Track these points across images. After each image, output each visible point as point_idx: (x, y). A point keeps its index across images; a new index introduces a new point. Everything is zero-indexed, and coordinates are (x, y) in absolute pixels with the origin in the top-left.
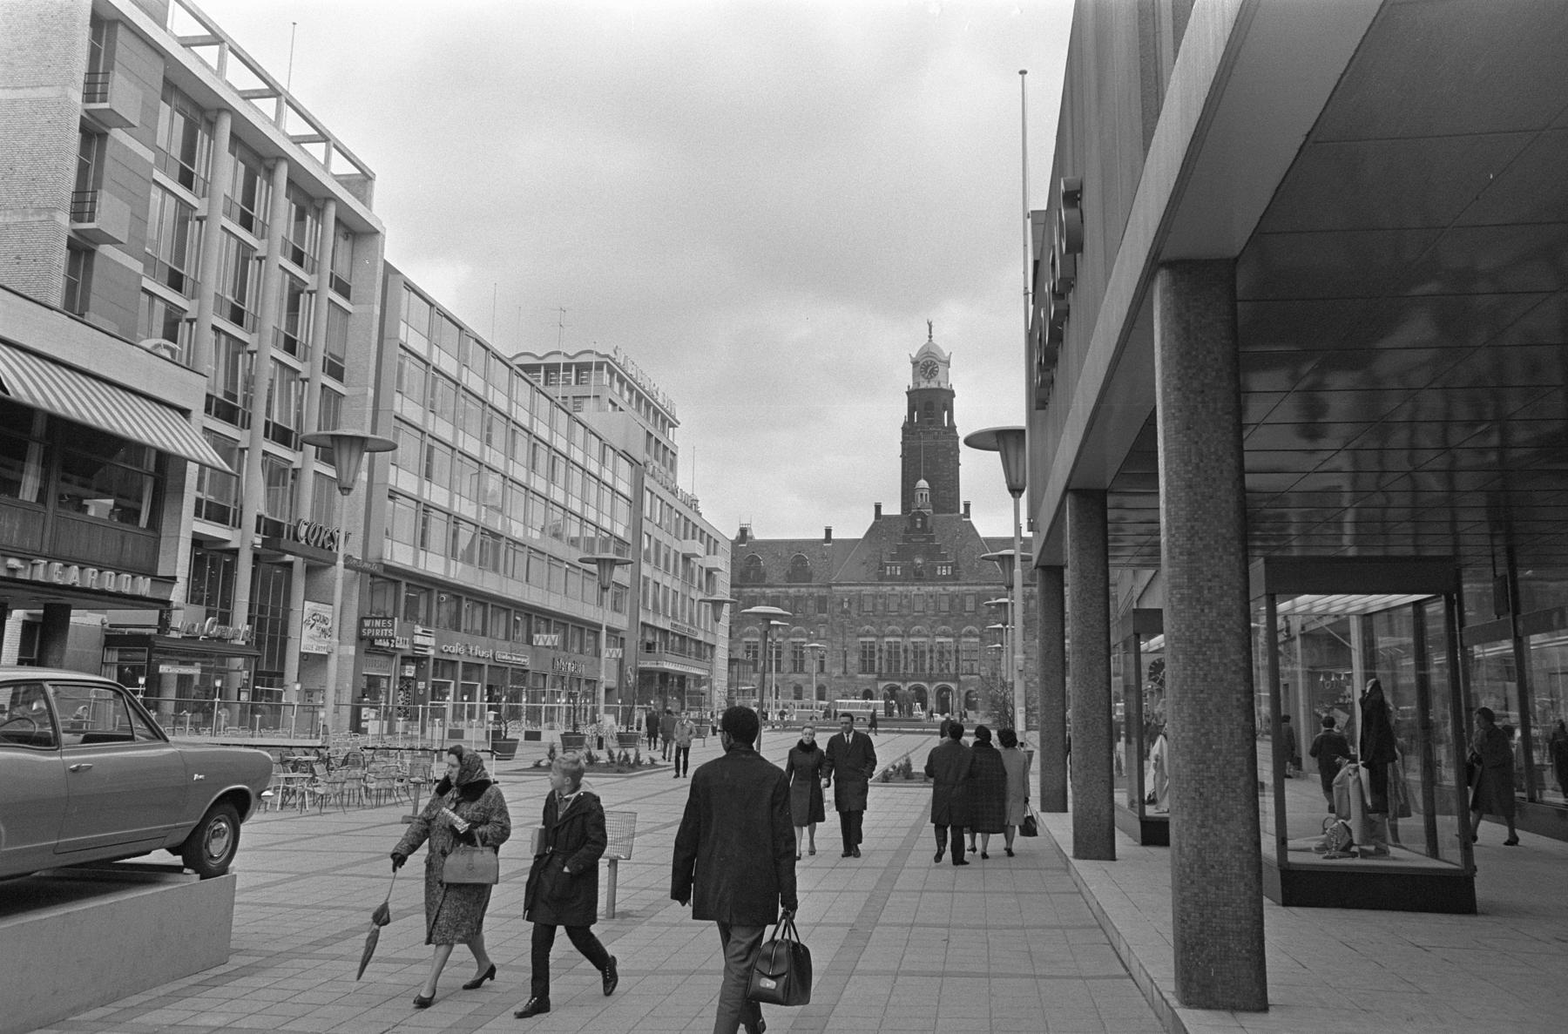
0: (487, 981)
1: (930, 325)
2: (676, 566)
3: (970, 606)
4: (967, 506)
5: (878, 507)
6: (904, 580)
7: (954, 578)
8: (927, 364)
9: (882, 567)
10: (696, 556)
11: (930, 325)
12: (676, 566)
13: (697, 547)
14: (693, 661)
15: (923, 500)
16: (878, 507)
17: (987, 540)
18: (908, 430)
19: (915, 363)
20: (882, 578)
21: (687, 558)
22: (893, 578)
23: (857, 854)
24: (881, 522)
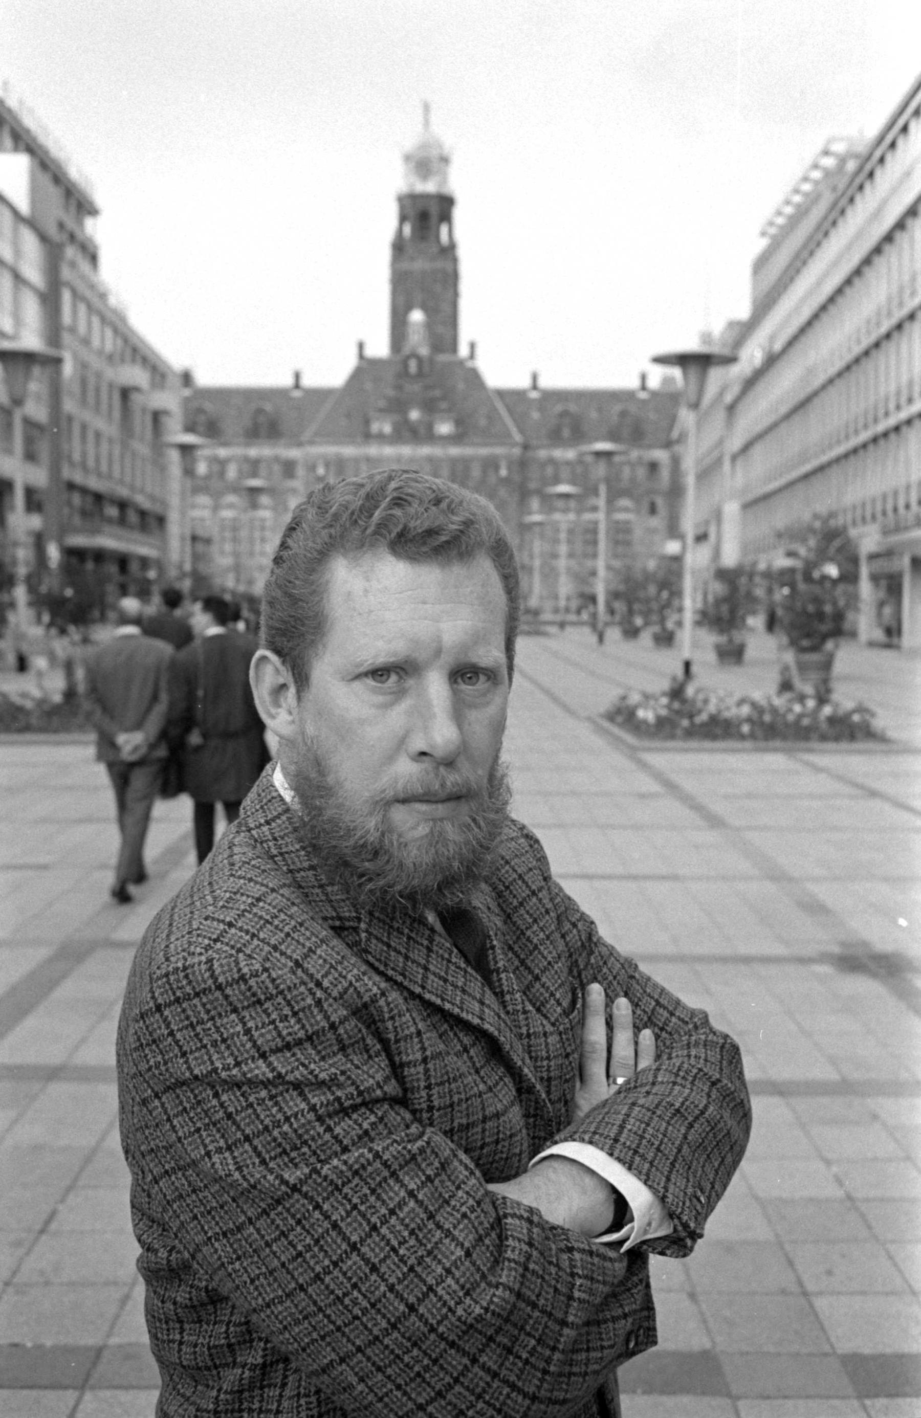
0: (893, 436)
1: (427, 108)
2: (110, 406)
3: (476, 472)
4: (472, 346)
5: (361, 346)
6: (397, 437)
7: (457, 439)
8: (427, 162)
9: (367, 422)
10: (137, 389)
11: (427, 108)
12: (110, 406)
13: (136, 375)
14: (136, 535)
15: (417, 340)
16: (361, 346)
17: (501, 394)
18: (399, 247)
19: (407, 158)
20: (367, 437)
21: (126, 393)
22: (381, 438)
23: (897, 647)
24: (367, 367)
